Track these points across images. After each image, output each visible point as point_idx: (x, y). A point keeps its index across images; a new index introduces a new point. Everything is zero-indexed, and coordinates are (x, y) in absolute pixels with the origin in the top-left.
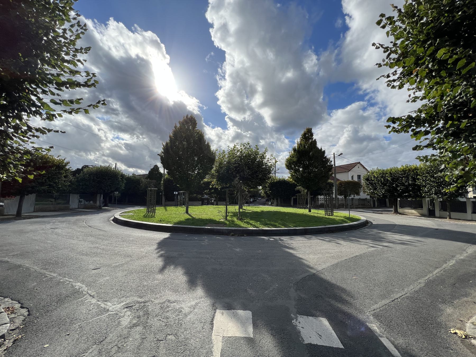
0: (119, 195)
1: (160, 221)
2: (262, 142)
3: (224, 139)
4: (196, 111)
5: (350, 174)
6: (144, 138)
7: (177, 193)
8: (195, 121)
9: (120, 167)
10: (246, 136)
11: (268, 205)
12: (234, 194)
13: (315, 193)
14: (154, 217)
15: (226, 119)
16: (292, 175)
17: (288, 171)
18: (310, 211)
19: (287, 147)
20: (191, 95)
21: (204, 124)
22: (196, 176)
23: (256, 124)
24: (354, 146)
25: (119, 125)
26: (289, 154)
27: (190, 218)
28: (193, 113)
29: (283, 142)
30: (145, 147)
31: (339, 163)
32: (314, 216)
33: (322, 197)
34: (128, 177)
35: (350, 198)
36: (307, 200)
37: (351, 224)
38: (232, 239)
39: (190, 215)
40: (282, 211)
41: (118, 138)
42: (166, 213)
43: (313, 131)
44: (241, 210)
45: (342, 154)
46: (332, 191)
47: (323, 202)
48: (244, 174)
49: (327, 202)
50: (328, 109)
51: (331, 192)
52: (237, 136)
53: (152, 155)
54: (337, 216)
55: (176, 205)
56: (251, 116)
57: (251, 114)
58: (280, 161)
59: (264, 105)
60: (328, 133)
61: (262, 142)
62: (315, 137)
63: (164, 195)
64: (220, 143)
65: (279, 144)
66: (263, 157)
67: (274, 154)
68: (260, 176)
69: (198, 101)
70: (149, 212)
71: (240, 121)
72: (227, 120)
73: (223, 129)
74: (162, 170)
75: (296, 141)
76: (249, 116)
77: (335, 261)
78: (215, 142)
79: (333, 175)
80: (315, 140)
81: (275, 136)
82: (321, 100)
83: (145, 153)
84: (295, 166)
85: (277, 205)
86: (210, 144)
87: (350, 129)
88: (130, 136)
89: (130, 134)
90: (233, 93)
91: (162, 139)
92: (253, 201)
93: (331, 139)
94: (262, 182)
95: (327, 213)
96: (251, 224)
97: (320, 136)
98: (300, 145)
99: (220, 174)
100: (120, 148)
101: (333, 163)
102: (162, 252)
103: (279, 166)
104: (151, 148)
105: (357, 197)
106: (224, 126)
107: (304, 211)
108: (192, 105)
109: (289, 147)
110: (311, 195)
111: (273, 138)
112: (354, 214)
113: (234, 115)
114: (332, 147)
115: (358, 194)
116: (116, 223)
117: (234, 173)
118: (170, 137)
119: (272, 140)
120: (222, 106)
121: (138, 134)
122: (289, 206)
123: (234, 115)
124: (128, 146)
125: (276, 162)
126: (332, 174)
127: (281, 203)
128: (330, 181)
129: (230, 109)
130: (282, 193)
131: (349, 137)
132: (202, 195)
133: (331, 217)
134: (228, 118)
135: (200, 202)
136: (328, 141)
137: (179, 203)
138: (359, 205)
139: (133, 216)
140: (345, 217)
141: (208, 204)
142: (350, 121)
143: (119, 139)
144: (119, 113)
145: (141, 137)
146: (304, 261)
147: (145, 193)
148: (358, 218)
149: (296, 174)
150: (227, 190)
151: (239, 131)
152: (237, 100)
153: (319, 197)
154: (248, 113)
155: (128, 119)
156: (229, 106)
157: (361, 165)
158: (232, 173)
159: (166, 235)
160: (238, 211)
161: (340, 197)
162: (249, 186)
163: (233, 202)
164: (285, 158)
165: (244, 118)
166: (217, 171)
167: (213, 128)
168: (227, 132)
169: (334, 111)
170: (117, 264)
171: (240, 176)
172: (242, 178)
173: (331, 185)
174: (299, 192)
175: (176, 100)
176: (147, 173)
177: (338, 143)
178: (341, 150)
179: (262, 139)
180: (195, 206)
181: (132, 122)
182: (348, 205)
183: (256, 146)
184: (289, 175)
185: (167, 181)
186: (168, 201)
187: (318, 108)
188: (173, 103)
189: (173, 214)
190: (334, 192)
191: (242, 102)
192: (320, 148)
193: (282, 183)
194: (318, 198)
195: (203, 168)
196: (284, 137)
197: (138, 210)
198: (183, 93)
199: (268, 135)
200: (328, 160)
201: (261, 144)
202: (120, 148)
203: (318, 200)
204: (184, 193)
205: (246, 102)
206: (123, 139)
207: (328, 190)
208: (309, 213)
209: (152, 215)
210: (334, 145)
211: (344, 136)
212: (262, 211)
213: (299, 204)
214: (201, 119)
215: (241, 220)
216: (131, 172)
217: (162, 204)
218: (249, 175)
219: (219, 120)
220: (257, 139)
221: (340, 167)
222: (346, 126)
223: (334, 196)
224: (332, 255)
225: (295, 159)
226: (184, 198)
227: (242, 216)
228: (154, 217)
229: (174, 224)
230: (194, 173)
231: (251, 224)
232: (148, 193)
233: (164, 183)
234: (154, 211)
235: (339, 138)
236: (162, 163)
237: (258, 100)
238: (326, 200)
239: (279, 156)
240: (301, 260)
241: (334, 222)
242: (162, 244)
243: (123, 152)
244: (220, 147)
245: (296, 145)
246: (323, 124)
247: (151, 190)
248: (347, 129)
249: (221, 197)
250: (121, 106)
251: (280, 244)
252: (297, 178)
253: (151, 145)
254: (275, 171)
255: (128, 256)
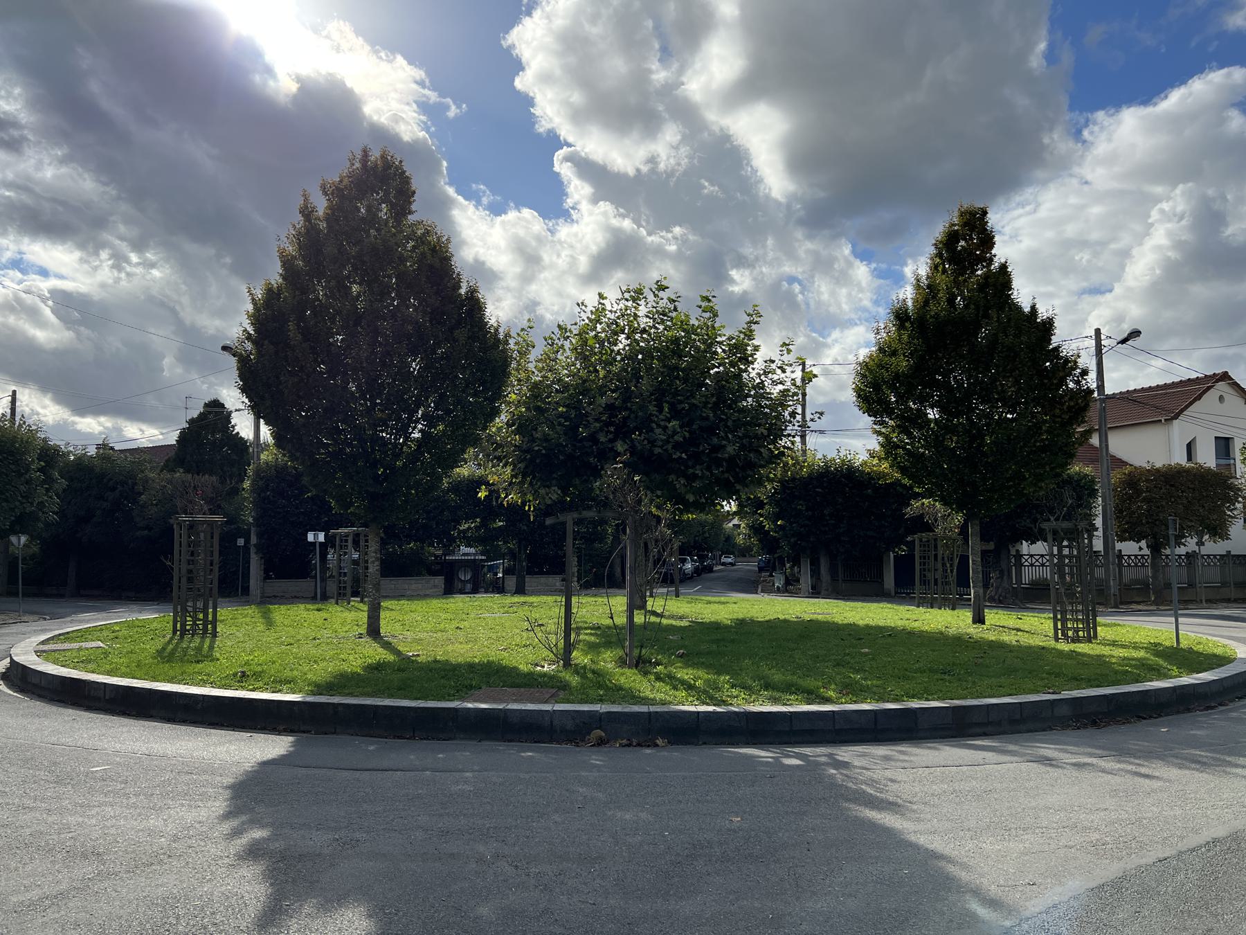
0: (35, 549)
1: (242, 678)
2: (741, 281)
3: (552, 266)
4: (410, 127)
5: (1180, 431)
6: (153, 265)
7: (321, 537)
8: (406, 181)
9: (34, 412)
10: (659, 252)
11: (769, 590)
12: (601, 538)
13: (1002, 535)
14: (210, 657)
15: (557, 168)
16: (889, 447)
17: (867, 420)
18: (979, 619)
19: (866, 300)
20: (385, 43)
21: (451, 191)
22: (415, 456)
23: (709, 188)
24: (1206, 292)
25: (25, 198)
26: (871, 337)
27: (391, 658)
28: (395, 139)
29: (842, 278)
30: (156, 307)
31: (1122, 376)
32: (1000, 646)
33: (1040, 548)
34: (80, 459)
35: (1182, 550)
36: (964, 560)
37: (1186, 680)
38: (596, 758)
39: (387, 646)
40: (839, 619)
41: (18, 264)
42: (270, 636)
43: (994, 219)
44: (639, 618)
45: (1135, 334)
46: (1089, 517)
47: (1046, 573)
48: (652, 442)
49: (1062, 576)
50: (1072, 108)
51: (1082, 525)
52: (620, 251)
53: (193, 347)
54: (1114, 644)
55: (320, 597)
56: (684, 150)
57: (685, 140)
58: (827, 373)
59: (749, 88)
60: (1071, 230)
61: (741, 281)
62: (1001, 252)
63: (259, 548)
64: (533, 287)
65: (823, 288)
66: (741, 352)
67: (800, 340)
68: (730, 449)
69: (420, 74)
70: (184, 632)
71: (631, 172)
72: (563, 169)
73: (545, 215)
74: (244, 425)
75: (908, 271)
76: (676, 148)
77: (1110, 870)
78: (510, 280)
79: (1095, 440)
80: (1004, 267)
81: (806, 246)
82: (1036, 61)
83: (161, 339)
84: (901, 398)
85: (816, 593)
86: (483, 294)
87: (1180, 208)
88: (77, 254)
89: (81, 246)
90: (595, 31)
91: (243, 268)
92: (698, 572)
93: (1083, 257)
94: (737, 475)
95: (1065, 629)
96: (689, 687)
97: (1027, 243)
98: (928, 292)
99: (533, 440)
100: (33, 314)
101: (1091, 380)
102: (258, 834)
103: (821, 400)
104: (189, 315)
105: (1212, 547)
106: (553, 205)
107: (952, 621)
108: (388, 94)
109: (876, 303)
110: (984, 537)
111: (792, 255)
112: (1202, 632)
113: (597, 145)
114: (1087, 298)
115: (1218, 530)
116: (21, 690)
117: (602, 438)
118: (287, 263)
119: (788, 269)
120: (539, 99)
121: (123, 246)
122: (874, 592)
123: (597, 145)
124: (69, 306)
125: (808, 378)
126: (1088, 433)
127: (834, 577)
128: (1075, 468)
129: (579, 117)
130: (839, 529)
131: (1178, 245)
132: (450, 543)
133: (1082, 648)
134: (567, 159)
135: (439, 581)
136: (1070, 269)
137: (332, 587)
138: (1224, 584)
139: (106, 654)
140: (1156, 649)
141: (475, 591)
142: (1177, 167)
143: (24, 272)
144: (23, 139)
145: (134, 258)
146: (951, 869)
147: (162, 540)
148: (1219, 651)
149: (910, 435)
150: (569, 518)
151: (627, 224)
152: (616, 66)
153: (1025, 547)
154: (671, 134)
155: (64, 170)
156: (577, 97)
157: (1236, 386)
158: (593, 438)
159: (274, 746)
160: (621, 620)
161: (1129, 548)
162: (678, 499)
163: (601, 577)
164: (851, 358)
165: (652, 160)
166: (521, 425)
167: (497, 210)
168: (564, 231)
169: (1100, 115)
170: (35, 894)
171: (632, 450)
172: (645, 462)
173: (1084, 490)
174: (921, 524)
175: (306, 71)
176: (172, 438)
177: (1118, 276)
178: (1135, 314)
179: (741, 262)
180: (411, 598)
181: (88, 186)
182: (1168, 586)
183: (707, 299)
184: (874, 443)
185: (275, 484)
186: (280, 576)
187: (1022, 102)
188: (293, 87)
189: (303, 642)
190: (1098, 522)
191: (640, 77)
192: (1027, 309)
193: (841, 481)
194: (1019, 556)
195: (448, 412)
196: (847, 250)
197: (130, 625)
198: (341, 30)
199: (770, 242)
200: (1066, 366)
201: (736, 289)
202: (33, 314)
203: (1019, 565)
204: (357, 535)
205: (660, 75)
206: (44, 273)
207: (1068, 517)
208: (975, 631)
209: (199, 649)
210: (1097, 291)
211: (1150, 243)
212: (741, 623)
213: (924, 582)
214: (434, 167)
215: (640, 664)
216: (90, 435)
217: (246, 591)
218: (677, 446)
219: (523, 168)
220: (713, 265)
221: (1128, 397)
222: (1159, 190)
223: (1098, 545)
224: (1096, 836)
225: (903, 364)
226: (355, 562)
227: (643, 645)
228: (210, 657)
229: (313, 694)
230: (407, 438)
231: (689, 687)
232: (181, 538)
233: (257, 490)
234: (209, 629)
235: (1125, 254)
236: (244, 390)
237: (717, 64)
238: (1060, 566)
239: (822, 344)
240: (943, 864)
241: (1100, 671)
242: (251, 794)
243: (47, 333)
244: (533, 305)
245: (907, 294)
246: (1044, 183)
247: (192, 526)
248: (1165, 206)
249: (533, 554)
250: (34, 103)
251: (833, 785)
252: (915, 460)
253: (185, 300)
254: (804, 425)
255: (84, 856)
